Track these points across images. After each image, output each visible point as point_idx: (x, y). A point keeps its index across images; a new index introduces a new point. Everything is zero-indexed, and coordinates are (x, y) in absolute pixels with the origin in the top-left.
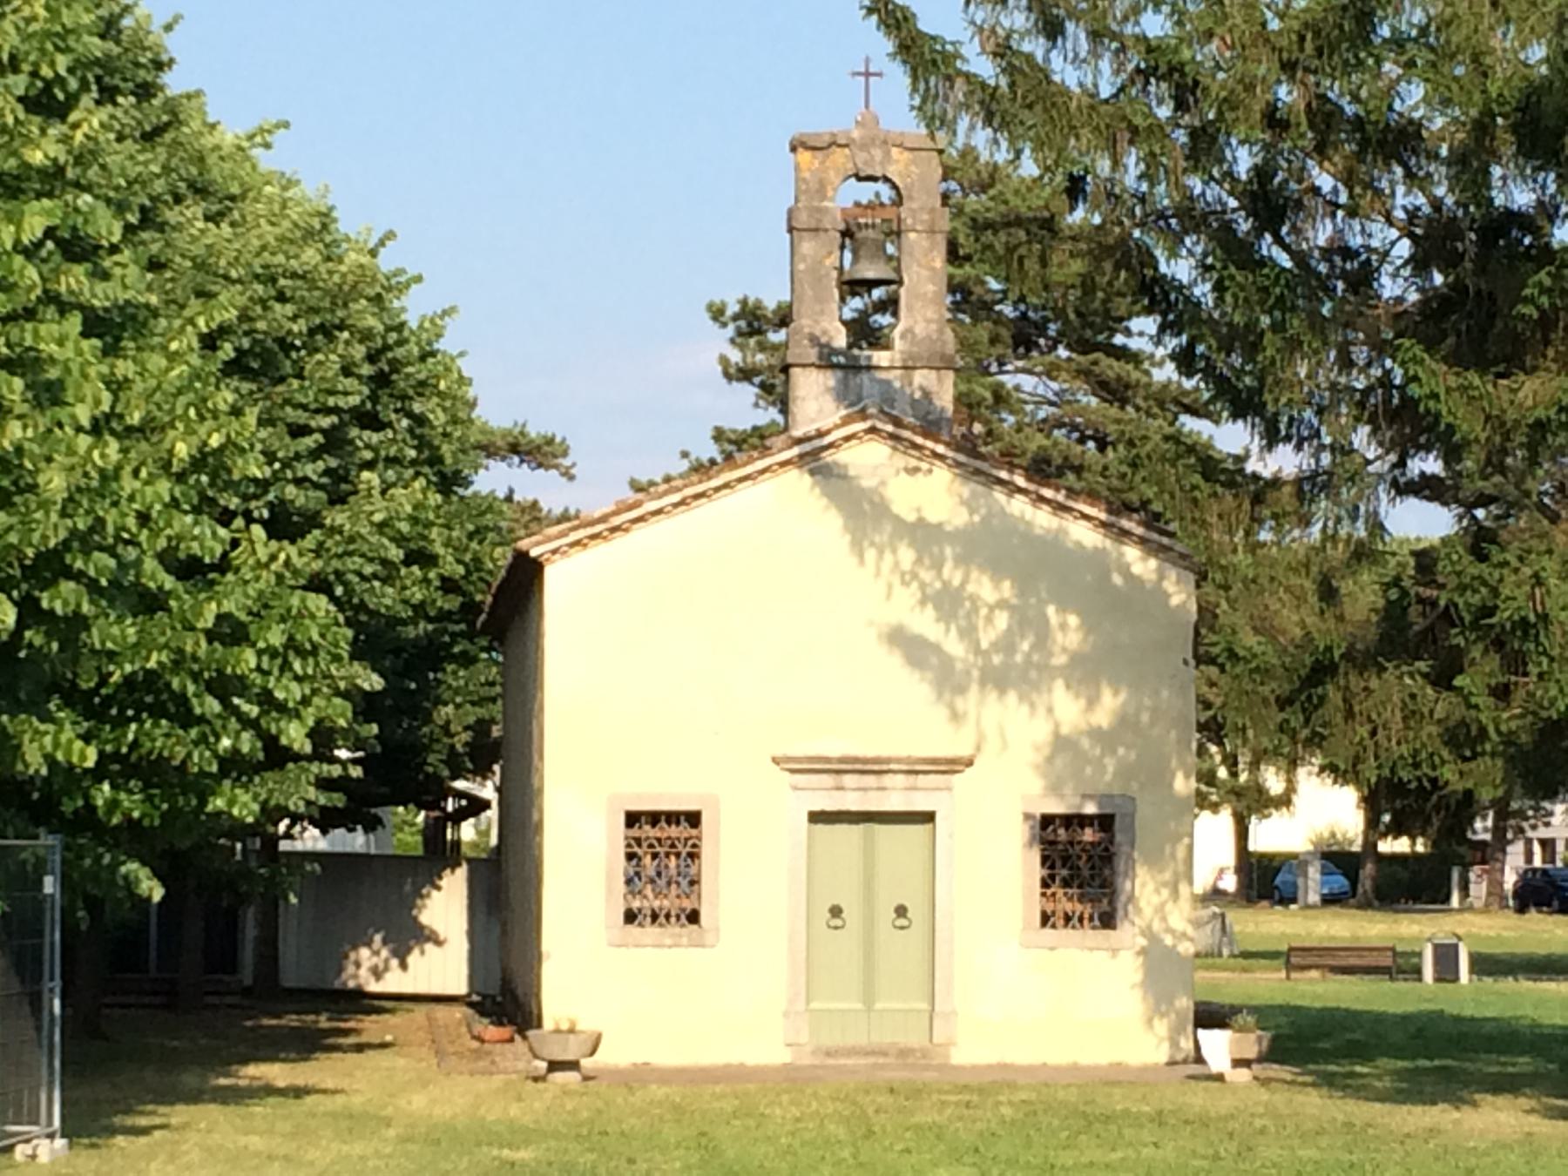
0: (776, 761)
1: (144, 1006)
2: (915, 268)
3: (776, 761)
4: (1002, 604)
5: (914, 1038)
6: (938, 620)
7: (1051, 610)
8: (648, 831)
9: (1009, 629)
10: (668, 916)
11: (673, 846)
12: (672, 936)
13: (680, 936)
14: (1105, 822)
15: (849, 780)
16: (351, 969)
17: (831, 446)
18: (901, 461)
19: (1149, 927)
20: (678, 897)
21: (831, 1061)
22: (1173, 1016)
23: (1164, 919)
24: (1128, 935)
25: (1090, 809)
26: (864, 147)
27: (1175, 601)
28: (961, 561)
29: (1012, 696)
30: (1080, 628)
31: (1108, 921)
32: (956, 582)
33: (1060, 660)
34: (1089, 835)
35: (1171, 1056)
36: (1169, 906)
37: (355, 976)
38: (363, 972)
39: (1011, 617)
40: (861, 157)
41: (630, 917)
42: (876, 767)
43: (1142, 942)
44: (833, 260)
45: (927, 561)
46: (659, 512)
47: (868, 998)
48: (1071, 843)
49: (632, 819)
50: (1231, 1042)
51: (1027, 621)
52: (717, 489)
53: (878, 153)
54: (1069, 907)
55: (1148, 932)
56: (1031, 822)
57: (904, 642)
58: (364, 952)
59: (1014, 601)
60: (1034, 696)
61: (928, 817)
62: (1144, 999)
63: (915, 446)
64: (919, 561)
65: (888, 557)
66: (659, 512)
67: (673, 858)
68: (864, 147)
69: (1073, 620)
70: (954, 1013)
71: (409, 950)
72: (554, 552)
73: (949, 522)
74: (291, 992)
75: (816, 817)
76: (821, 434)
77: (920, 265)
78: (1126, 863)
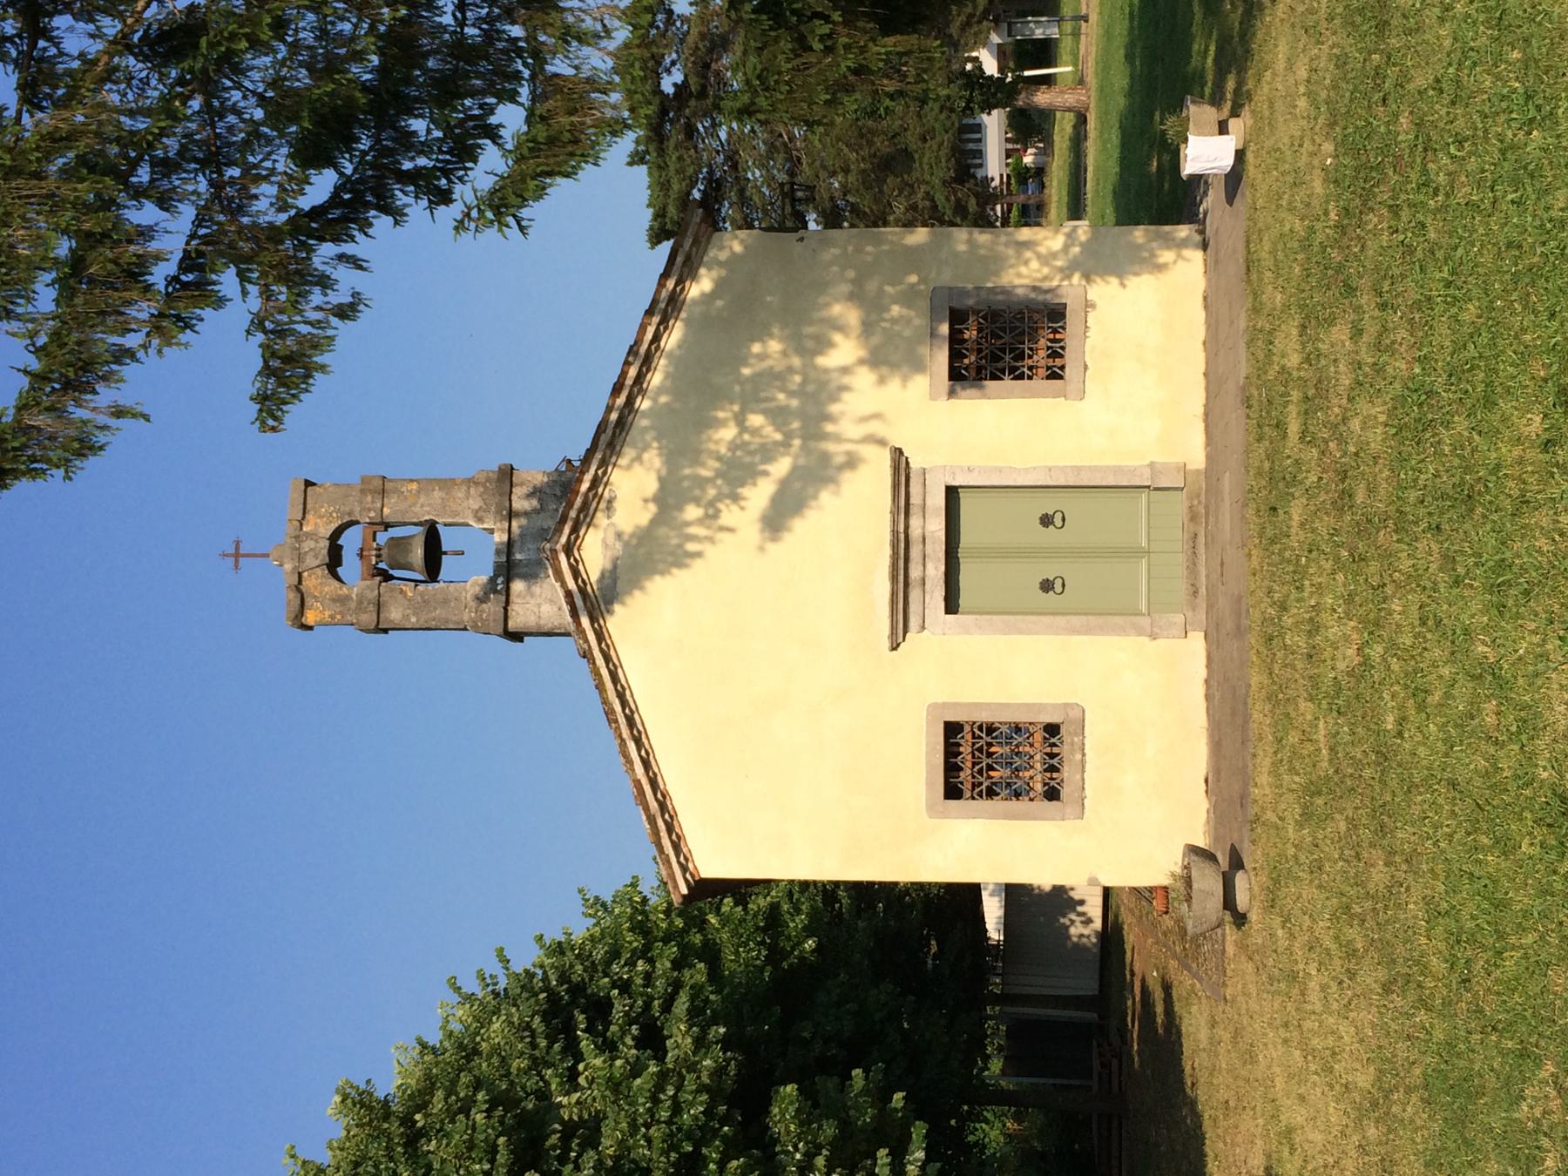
0: (895, 647)
1: (1120, 1125)
2: (417, 509)
3: (895, 647)
4: (740, 420)
5: (1177, 506)
6: (755, 484)
7: (746, 371)
8: (965, 775)
9: (764, 412)
10: (1052, 756)
11: (980, 750)
12: (1072, 752)
13: (1072, 743)
14: (957, 318)
15: (915, 573)
16: (1084, 940)
17: (582, 591)
18: (600, 518)
19: (1061, 270)
20: (1031, 745)
21: (1203, 590)
22: (1154, 245)
23: (1054, 255)
24: (1070, 290)
25: (944, 329)
26: (300, 558)
27: (737, 248)
28: (696, 457)
29: (834, 408)
30: (761, 340)
31: (1057, 314)
32: (717, 465)
33: (796, 361)
34: (971, 334)
35: (1196, 247)
36: (1042, 250)
37: (1088, 937)
38: (1086, 932)
39: (754, 412)
40: (311, 561)
41: (1052, 794)
42: (902, 545)
43: (1076, 279)
44: (408, 588)
45: (697, 492)
46: (646, 764)
47: (1138, 553)
48: (979, 351)
49: (952, 792)
50: (1199, 134)
51: (753, 395)
52: (624, 703)
53: (307, 545)
54: (1042, 353)
55: (1067, 273)
56: (958, 388)
57: (775, 522)
58: (1073, 931)
59: (736, 408)
60: (833, 385)
61: (952, 493)
62: (1136, 274)
63: (585, 506)
64: (697, 501)
65: (692, 530)
66: (646, 764)
67: (993, 749)
68: (300, 558)
69: (756, 348)
70: (1152, 465)
71: (1071, 899)
72: (684, 869)
73: (658, 471)
74: (1101, 991)
75: (951, 606)
76: (569, 595)
77: (415, 504)
78: (997, 294)
